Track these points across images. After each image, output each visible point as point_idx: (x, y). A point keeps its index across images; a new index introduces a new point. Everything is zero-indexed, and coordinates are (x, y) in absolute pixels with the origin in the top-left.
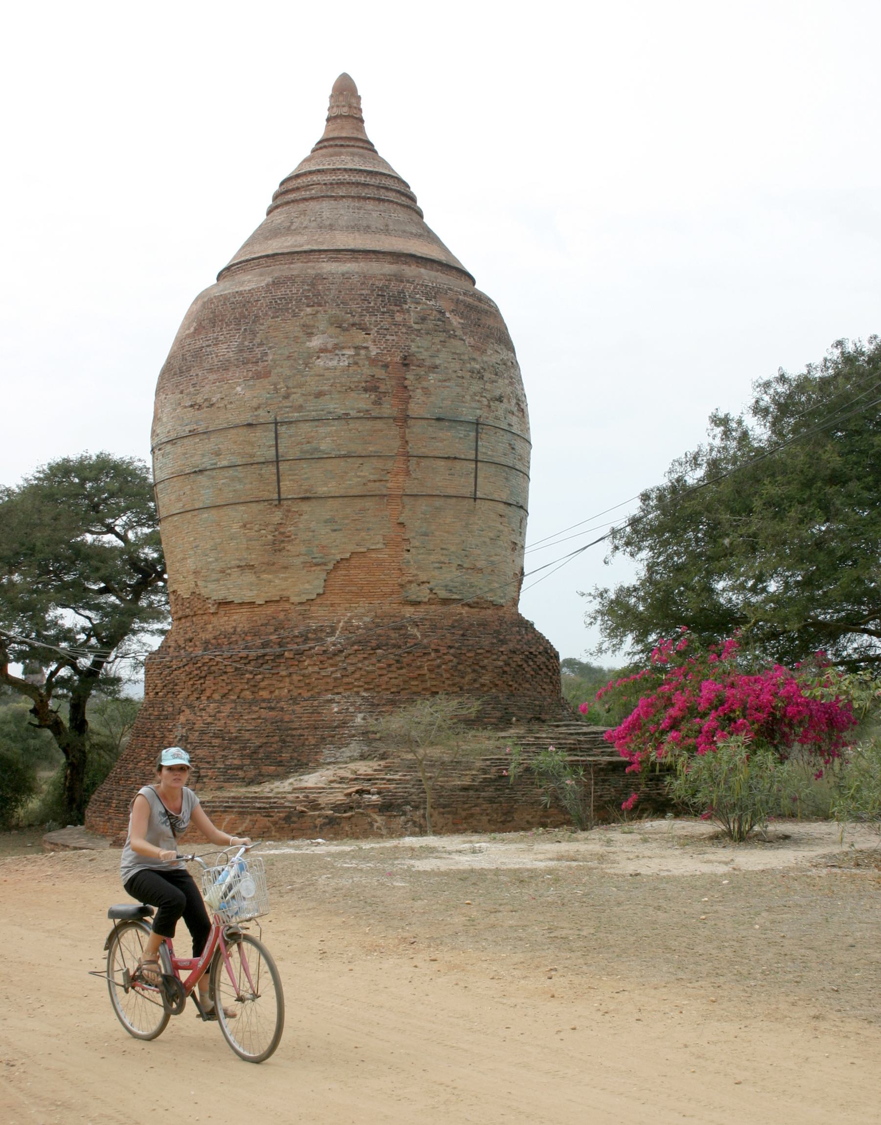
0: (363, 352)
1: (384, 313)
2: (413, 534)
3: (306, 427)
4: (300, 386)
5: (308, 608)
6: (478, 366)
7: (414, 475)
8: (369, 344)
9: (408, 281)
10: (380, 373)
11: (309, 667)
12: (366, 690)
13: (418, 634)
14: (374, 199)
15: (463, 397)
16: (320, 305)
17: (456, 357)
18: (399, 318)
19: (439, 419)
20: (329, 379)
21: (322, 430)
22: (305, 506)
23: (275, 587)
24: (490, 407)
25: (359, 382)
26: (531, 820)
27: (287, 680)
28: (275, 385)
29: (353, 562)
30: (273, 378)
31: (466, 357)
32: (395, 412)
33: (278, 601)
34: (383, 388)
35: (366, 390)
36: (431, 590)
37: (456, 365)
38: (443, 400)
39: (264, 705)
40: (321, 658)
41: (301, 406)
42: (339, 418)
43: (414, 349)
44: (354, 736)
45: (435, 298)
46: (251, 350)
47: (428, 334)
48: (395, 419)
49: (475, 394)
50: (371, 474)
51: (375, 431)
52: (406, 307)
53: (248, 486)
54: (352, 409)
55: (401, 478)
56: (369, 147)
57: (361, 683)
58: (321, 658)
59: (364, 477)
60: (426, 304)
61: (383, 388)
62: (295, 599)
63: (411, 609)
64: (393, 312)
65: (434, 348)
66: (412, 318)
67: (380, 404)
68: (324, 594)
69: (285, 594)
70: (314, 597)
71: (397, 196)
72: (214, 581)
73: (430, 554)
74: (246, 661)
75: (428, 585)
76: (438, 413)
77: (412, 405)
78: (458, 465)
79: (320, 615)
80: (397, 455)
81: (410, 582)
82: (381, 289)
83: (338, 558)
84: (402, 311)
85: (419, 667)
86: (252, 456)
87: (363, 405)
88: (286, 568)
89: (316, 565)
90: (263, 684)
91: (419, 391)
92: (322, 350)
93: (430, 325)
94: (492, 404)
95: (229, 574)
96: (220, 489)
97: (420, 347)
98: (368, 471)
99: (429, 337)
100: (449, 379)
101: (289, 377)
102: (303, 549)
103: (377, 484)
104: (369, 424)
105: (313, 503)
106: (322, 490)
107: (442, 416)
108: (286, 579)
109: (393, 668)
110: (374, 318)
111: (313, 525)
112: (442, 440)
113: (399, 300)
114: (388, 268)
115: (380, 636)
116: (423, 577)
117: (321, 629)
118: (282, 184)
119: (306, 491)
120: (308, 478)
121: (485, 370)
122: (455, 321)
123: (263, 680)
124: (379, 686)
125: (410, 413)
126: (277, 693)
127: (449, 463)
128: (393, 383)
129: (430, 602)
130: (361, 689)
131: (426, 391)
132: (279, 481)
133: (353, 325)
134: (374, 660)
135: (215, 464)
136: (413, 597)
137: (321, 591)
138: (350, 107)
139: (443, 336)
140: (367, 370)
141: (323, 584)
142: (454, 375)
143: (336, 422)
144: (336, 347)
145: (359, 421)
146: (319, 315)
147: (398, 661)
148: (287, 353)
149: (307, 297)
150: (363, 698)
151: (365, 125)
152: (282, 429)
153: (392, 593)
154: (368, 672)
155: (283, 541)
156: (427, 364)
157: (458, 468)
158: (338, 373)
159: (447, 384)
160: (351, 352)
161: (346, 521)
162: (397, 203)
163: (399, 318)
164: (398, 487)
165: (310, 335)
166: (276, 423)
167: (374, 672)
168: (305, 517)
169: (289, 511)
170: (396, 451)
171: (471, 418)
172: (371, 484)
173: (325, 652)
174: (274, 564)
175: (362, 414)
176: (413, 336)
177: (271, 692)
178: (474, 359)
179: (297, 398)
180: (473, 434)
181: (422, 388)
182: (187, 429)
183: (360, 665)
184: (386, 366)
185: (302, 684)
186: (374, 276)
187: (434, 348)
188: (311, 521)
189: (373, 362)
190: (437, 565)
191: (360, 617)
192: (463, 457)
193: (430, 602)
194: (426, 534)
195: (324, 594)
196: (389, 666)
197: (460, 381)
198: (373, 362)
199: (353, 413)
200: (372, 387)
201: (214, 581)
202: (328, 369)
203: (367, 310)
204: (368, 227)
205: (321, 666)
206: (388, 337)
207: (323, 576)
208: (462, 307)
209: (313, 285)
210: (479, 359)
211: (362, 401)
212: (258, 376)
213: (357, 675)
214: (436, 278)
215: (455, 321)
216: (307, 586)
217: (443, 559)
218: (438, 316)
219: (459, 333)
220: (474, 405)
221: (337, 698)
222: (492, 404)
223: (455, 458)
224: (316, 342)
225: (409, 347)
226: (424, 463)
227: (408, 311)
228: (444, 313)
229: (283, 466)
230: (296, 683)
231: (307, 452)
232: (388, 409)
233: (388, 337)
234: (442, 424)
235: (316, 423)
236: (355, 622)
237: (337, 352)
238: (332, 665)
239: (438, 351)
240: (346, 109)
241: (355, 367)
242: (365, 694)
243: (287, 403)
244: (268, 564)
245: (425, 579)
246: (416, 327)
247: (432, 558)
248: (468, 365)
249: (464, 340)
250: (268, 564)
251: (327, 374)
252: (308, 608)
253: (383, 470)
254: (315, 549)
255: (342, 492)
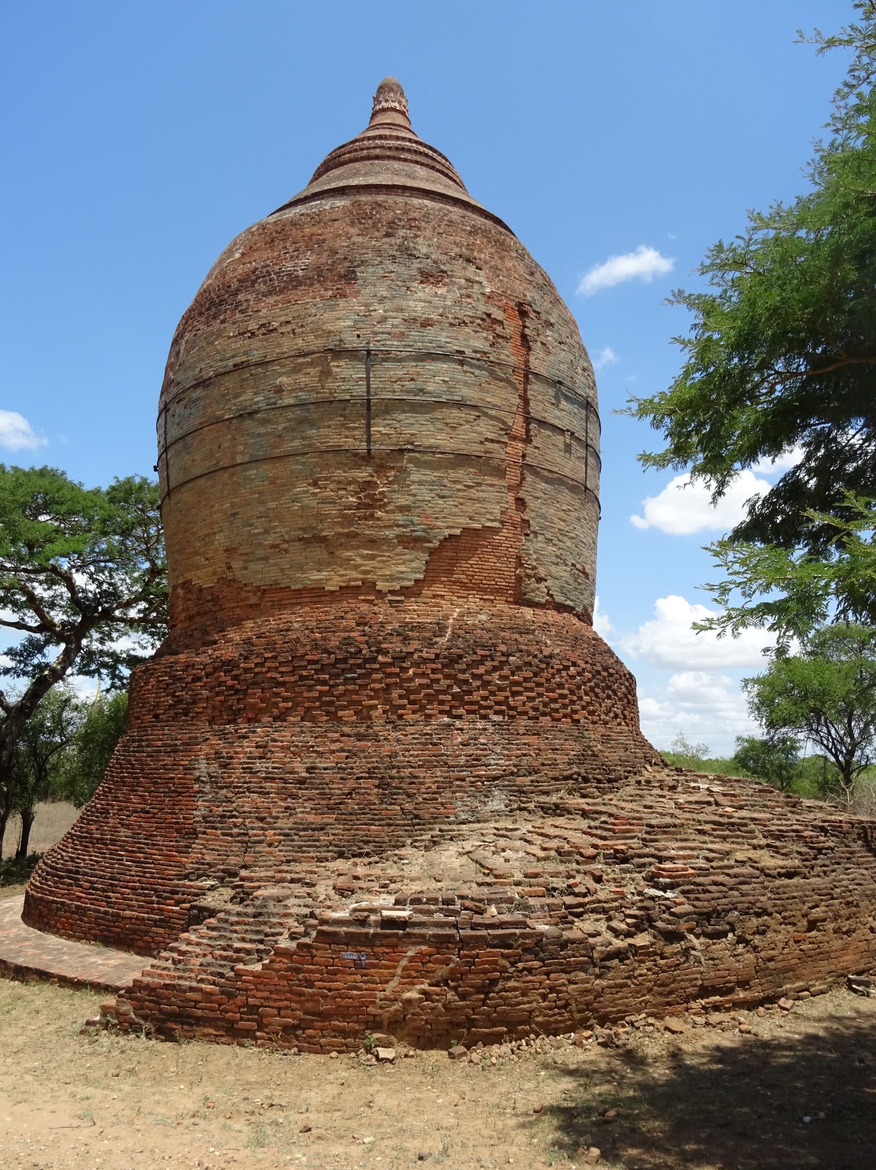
0: (476, 286)
12: (497, 713)
20: (437, 308)
41: (402, 334)
59: (480, 433)
72: (261, 559)
74: (318, 666)
85: (561, 686)
87: (479, 344)
91: (539, 344)
95: (286, 551)
96: (280, 436)
135: (274, 403)
150: (494, 724)
175: (479, 355)
182: (230, 363)
201: (261, 559)
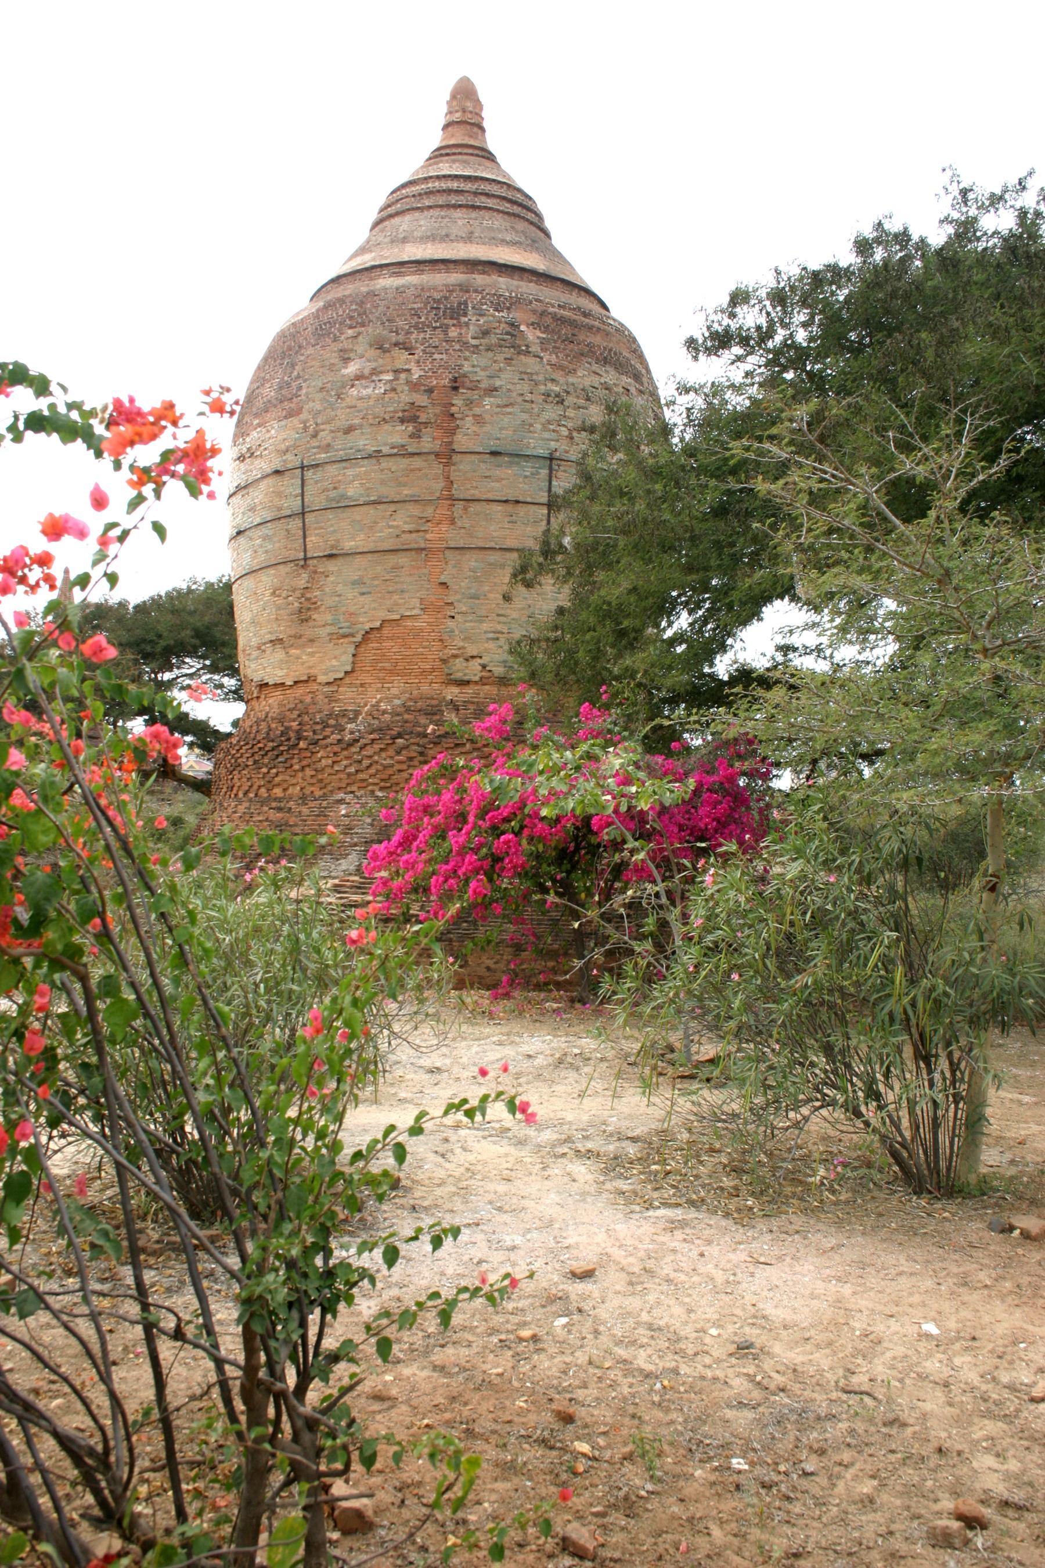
1: (435, 328)
2: (458, 597)
3: (332, 470)
4: (328, 422)
5: (335, 688)
6: (557, 389)
7: (459, 523)
8: (412, 366)
9: (476, 291)
10: (422, 400)
11: (323, 757)
12: (382, 789)
13: (456, 721)
14: (467, 206)
15: (531, 425)
16: (363, 325)
17: (525, 377)
18: (453, 333)
19: (494, 453)
21: (350, 472)
22: (331, 566)
23: (303, 664)
24: (572, 438)
25: (395, 412)
26: (493, 966)
27: (300, 774)
28: (304, 422)
29: (385, 632)
30: (304, 416)
31: (541, 378)
32: (437, 446)
33: (306, 681)
34: (423, 418)
35: (402, 421)
36: (484, 667)
37: (525, 387)
38: (501, 429)
39: (274, 805)
40: (336, 749)
41: (329, 445)
42: (370, 457)
43: (467, 368)
44: (356, 845)
45: (508, 309)
46: (289, 385)
47: (488, 350)
48: (437, 455)
49: (549, 422)
50: (405, 523)
51: (412, 470)
52: (464, 319)
53: (277, 545)
54: (385, 444)
55: (444, 527)
56: (489, 157)
57: (376, 781)
58: (336, 749)
59: (397, 527)
60: (493, 316)
61: (423, 418)
62: (322, 679)
63: (455, 690)
64: (447, 326)
65: (496, 367)
66: (470, 335)
67: (419, 437)
68: (352, 671)
69: (313, 672)
70: (341, 675)
71: (520, 210)
73: (481, 622)
75: (479, 661)
76: (493, 445)
77: (459, 437)
78: (522, 510)
79: (347, 696)
80: (439, 498)
81: (455, 656)
82: (438, 301)
83: (367, 627)
84: (459, 325)
86: (280, 509)
88: (312, 641)
89: (344, 636)
90: (277, 780)
92: (358, 378)
93: (493, 339)
94: (575, 434)
97: (474, 366)
98: (402, 520)
99: (490, 354)
100: (512, 404)
101: (320, 412)
102: (329, 618)
103: (414, 535)
104: (404, 462)
105: (340, 561)
106: (349, 545)
107: (499, 449)
108: (312, 654)
109: (416, 762)
110: (422, 335)
111: (339, 588)
112: (499, 480)
113: (457, 312)
114: (455, 277)
115: (406, 722)
116: (472, 650)
117: (344, 714)
118: (381, 210)
119: (332, 547)
120: (334, 531)
121: (568, 393)
122: (532, 335)
123: (277, 775)
124: (397, 784)
125: (455, 446)
126: (290, 791)
127: (509, 508)
128: (437, 411)
129: (482, 682)
130: (376, 788)
131: (479, 420)
132: (305, 537)
133: (396, 345)
134: (391, 752)
136: (459, 675)
137: (349, 668)
138: (464, 111)
139: (509, 353)
140: (406, 397)
141: (350, 659)
142: (520, 399)
143: (366, 462)
144: (375, 372)
145: (393, 459)
146: (360, 338)
147: (421, 754)
148: (320, 385)
149: (351, 318)
150: (378, 799)
151: (487, 134)
152: (309, 474)
153: (433, 670)
154: (385, 767)
155: (309, 609)
156: (483, 385)
157: (522, 514)
158: (371, 403)
159: (508, 410)
160: (389, 377)
161: (376, 582)
162: (498, 211)
163: (453, 333)
164: (440, 539)
165: (346, 360)
166: (302, 468)
167: (392, 766)
168: (332, 578)
169: (315, 572)
170: (438, 494)
171: (540, 452)
172: (406, 537)
173: (339, 741)
174: (300, 637)
176: (467, 354)
177: (285, 790)
178: (553, 380)
179: (325, 436)
180: (544, 472)
181: (474, 415)
183: (376, 758)
184: (430, 391)
185: (314, 781)
186: (435, 288)
187: (496, 367)
188: (339, 584)
189: (414, 387)
190: (491, 635)
191: (389, 700)
192: (529, 500)
193: (482, 682)
194: (475, 597)
195: (352, 671)
196: (411, 759)
197: (528, 405)
198: (414, 387)
199: (386, 450)
200: (410, 416)
202: (361, 398)
203: (416, 327)
204: (447, 236)
205: (335, 759)
206: (436, 356)
207: (351, 650)
208: (548, 320)
209: (361, 304)
210: (562, 380)
211: (398, 435)
212: (290, 414)
213: (372, 771)
214: (518, 287)
215: (532, 335)
216: (334, 662)
217: (499, 627)
218: (508, 329)
219: (535, 348)
220: (546, 435)
221: (349, 798)
222: (575, 434)
223: (517, 502)
224: (352, 369)
225: (461, 366)
226: (473, 508)
227: (467, 324)
228: (518, 327)
229: (309, 518)
230: (308, 778)
231: (333, 500)
232: (428, 442)
233: (436, 356)
234: (500, 458)
235: (344, 464)
236: (383, 706)
237: (374, 378)
238: (347, 758)
239: (500, 370)
240: (458, 115)
241: (392, 395)
242: (380, 794)
243: (315, 443)
244: (295, 637)
245: (475, 654)
246: (474, 342)
247: (485, 626)
248: (543, 387)
249: (541, 358)
250: (295, 637)
251: (359, 404)
252: (335, 688)
253: (421, 518)
254: (341, 618)
255: (371, 547)
